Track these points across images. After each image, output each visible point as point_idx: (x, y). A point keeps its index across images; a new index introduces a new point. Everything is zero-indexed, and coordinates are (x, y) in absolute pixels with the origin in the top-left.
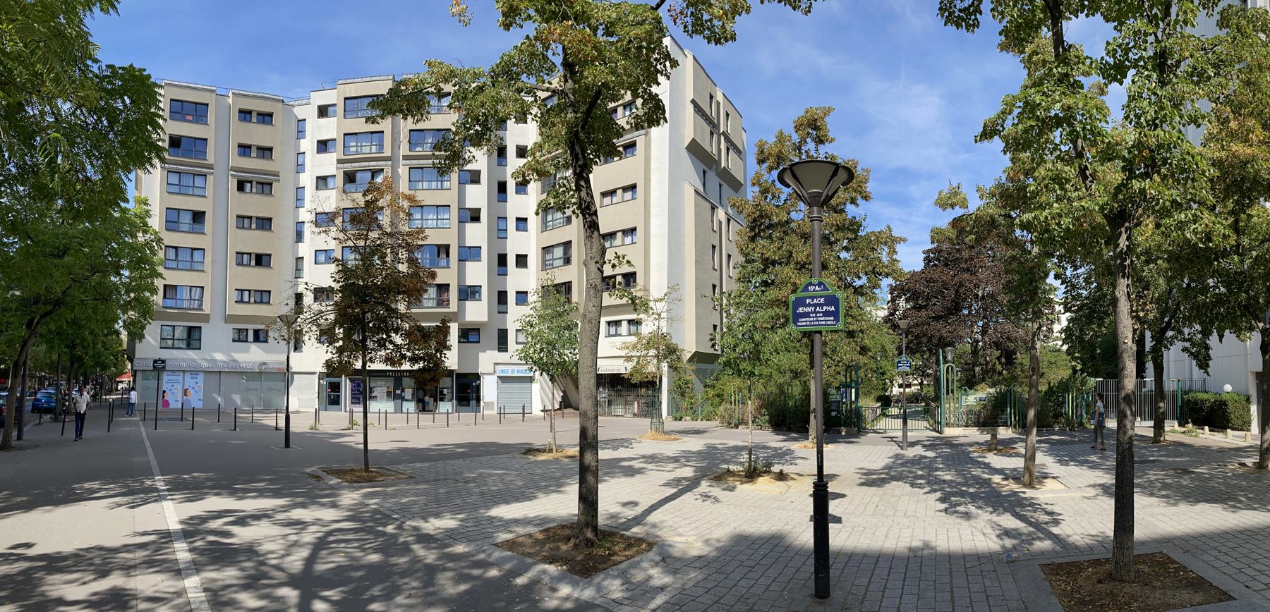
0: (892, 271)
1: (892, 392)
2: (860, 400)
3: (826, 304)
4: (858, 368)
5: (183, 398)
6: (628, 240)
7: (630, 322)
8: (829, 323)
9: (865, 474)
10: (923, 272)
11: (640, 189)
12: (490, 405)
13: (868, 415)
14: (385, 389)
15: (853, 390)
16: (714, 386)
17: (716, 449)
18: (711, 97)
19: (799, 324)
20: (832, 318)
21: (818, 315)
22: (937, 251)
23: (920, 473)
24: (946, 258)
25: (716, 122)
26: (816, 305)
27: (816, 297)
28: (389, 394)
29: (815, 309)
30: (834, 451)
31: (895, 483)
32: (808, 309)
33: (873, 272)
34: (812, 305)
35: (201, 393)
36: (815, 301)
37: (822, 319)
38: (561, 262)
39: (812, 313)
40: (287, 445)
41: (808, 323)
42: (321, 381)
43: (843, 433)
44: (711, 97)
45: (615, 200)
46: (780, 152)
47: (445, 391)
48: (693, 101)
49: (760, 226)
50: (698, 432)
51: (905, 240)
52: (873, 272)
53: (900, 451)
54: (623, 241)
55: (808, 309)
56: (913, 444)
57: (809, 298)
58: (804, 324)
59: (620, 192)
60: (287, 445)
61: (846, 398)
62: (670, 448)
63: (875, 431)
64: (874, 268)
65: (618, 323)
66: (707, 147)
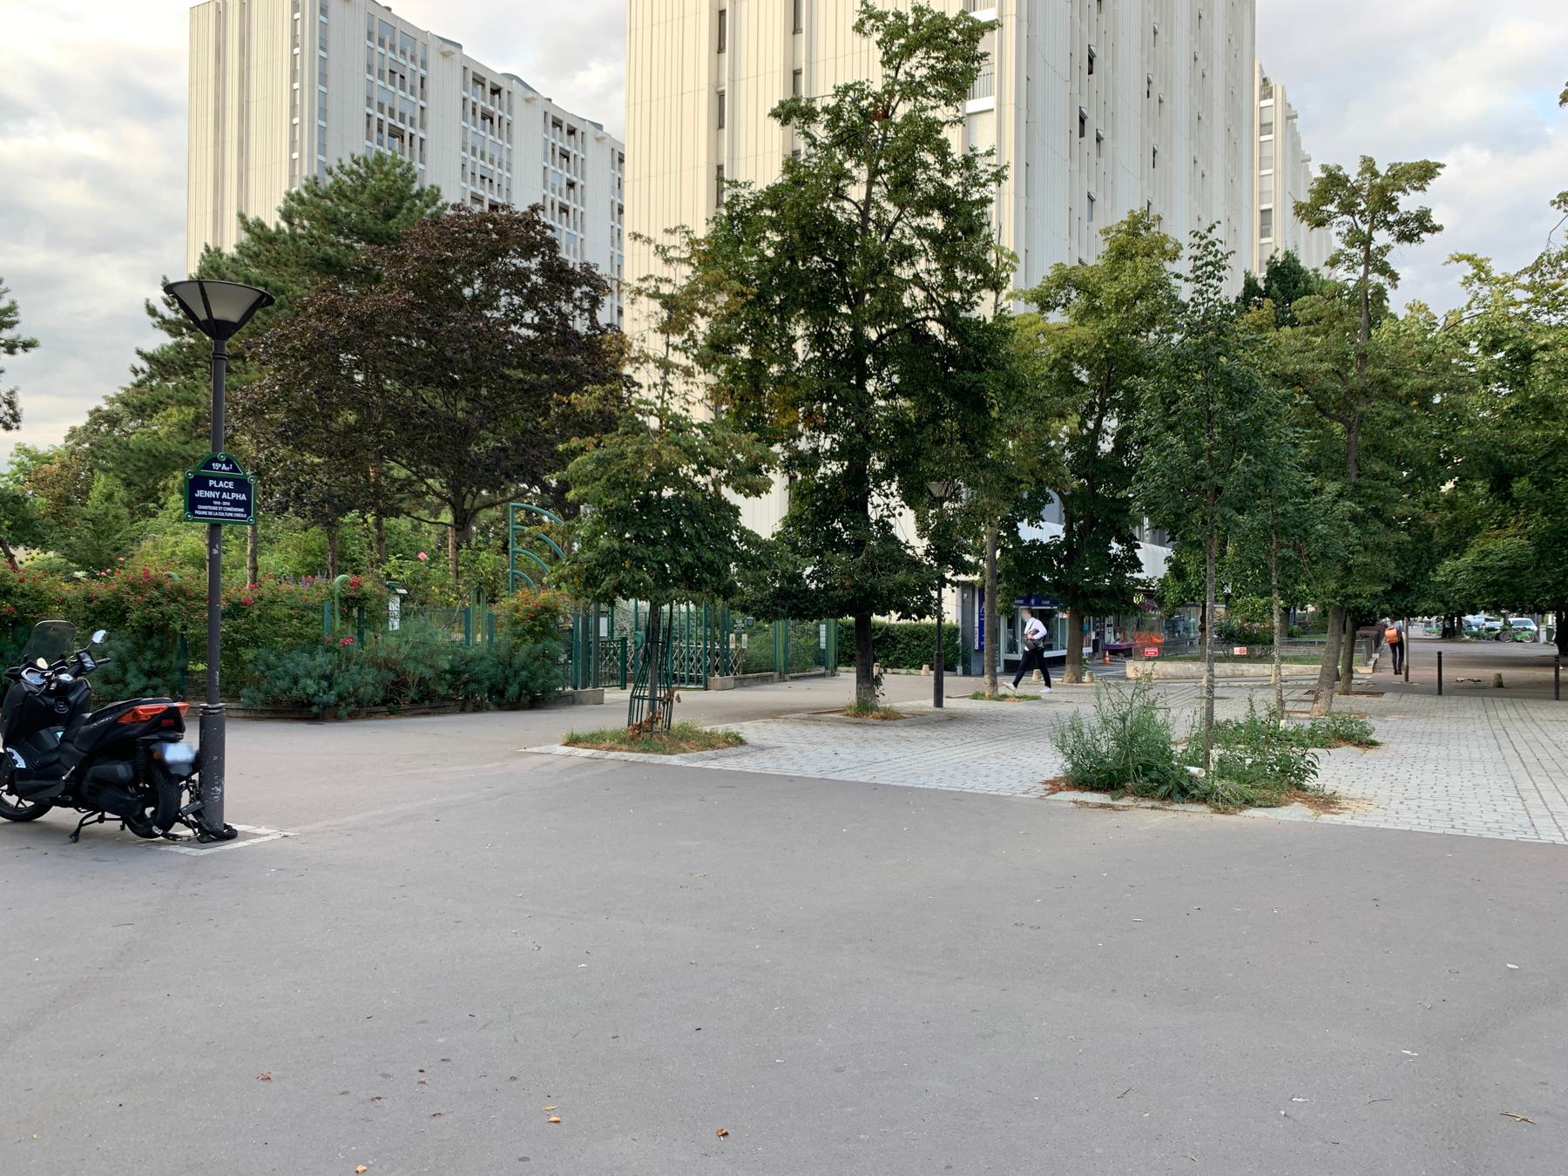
26: (222, 490)
32: (210, 494)
39: (216, 499)
55: (210, 494)
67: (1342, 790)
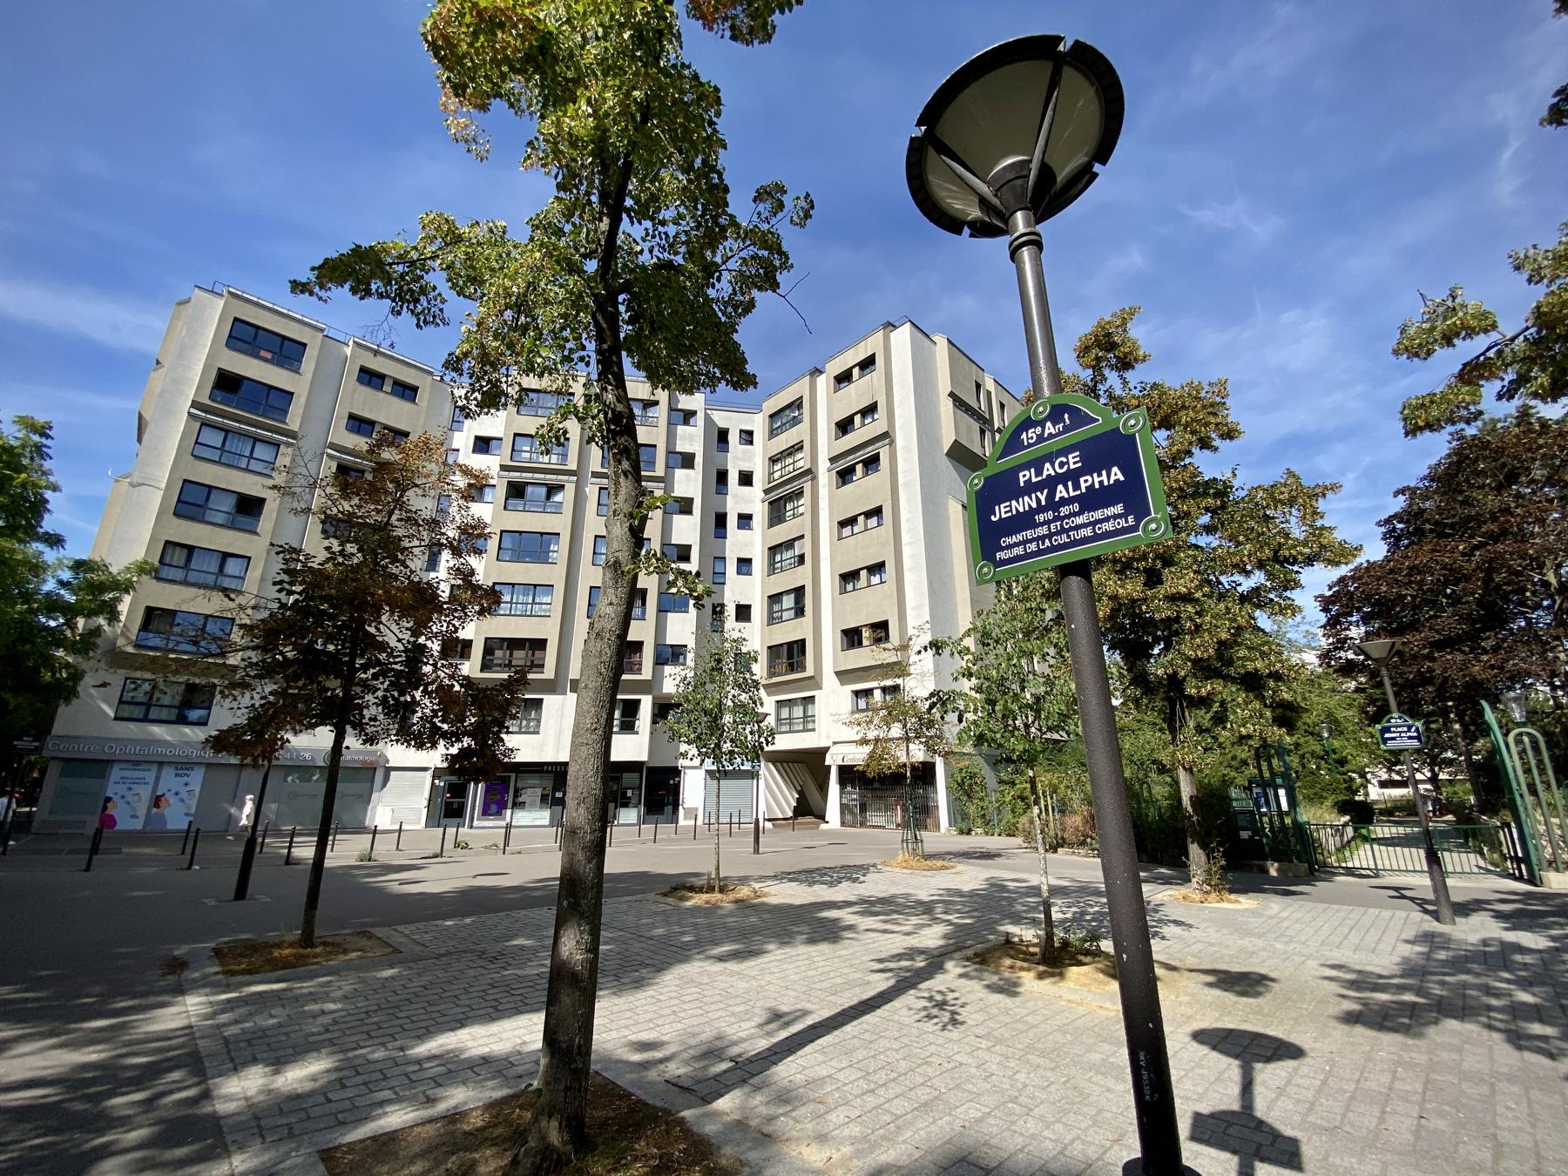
0: (1323, 551)
1: (1367, 794)
2: (1300, 810)
3: (1089, 467)
4: (1281, 751)
5: (149, 809)
6: (875, 579)
7: (884, 690)
8: (1109, 526)
9: (1353, 985)
10: (1387, 559)
11: (887, 513)
12: (692, 814)
13: (1330, 842)
14: (539, 791)
15: (1282, 792)
16: (1013, 784)
17: (1004, 888)
18: (978, 386)
19: (1000, 555)
21: (1064, 511)
22: (1411, 516)
23: (1525, 997)
24: (1437, 523)
26: (1051, 483)
27: (1050, 459)
28: (544, 798)
29: (1051, 496)
30: (1253, 913)
31: (1452, 1024)
32: (1027, 502)
33: (1276, 559)
34: (1039, 487)
35: (193, 803)
36: (1048, 470)
37: (1079, 520)
38: (792, 613)
39: (1041, 509)
40: (241, 892)
41: (1033, 547)
42: (436, 781)
43: (1273, 873)
44: (978, 386)
45: (856, 530)
47: (629, 793)
48: (952, 395)
50: (987, 856)
51: (1334, 488)
52: (1276, 559)
53: (1434, 926)
54: (869, 580)
55: (1027, 502)
56: (1465, 909)
57: (1026, 466)
58: (1019, 551)
59: (861, 519)
60: (241, 892)
61: (1268, 804)
62: (926, 885)
63: (1350, 872)
64: (1276, 552)
65: (868, 693)
66: (977, 450)
67: (1305, 1047)
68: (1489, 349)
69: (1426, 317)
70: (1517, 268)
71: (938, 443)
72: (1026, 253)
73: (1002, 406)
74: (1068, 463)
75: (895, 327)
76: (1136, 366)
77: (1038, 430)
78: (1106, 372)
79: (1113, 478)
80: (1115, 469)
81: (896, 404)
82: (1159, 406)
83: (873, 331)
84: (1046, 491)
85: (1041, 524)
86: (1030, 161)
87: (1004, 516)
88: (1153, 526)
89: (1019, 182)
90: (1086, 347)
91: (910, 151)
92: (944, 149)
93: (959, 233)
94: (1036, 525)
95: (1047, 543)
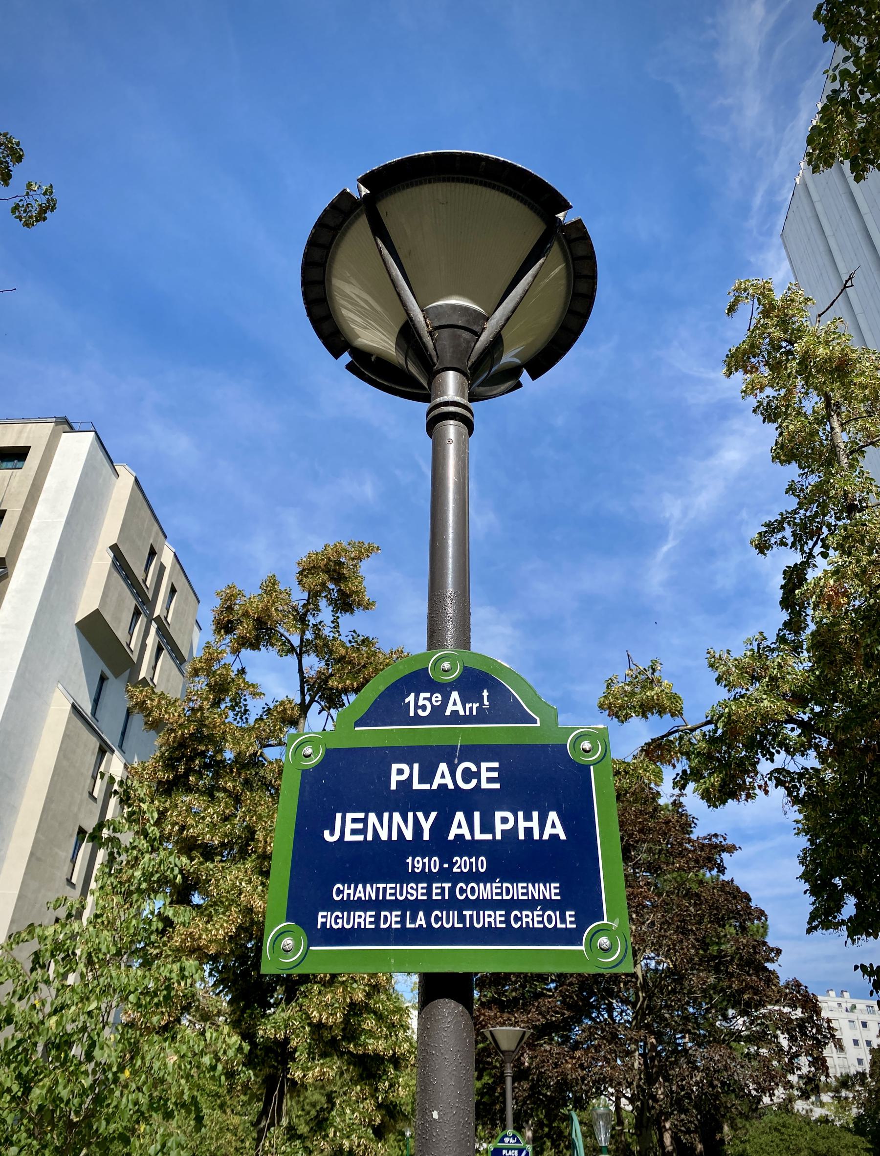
8: (531, 919)
18: (152, 553)
19: (325, 918)
20: (551, 891)
21: (461, 864)
25: (150, 596)
29: (442, 826)
36: (443, 776)
37: (485, 891)
39: (418, 847)
41: (392, 919)
44: (152, 553)
46: (267, 609)
48: (114, 548)
49: (191, 759)
57: (407, 755)
58: (364, 919)
66: (121, 634)
68: (670, 734)
69: (628, 680)
70: (711, 666)
71: (72, 604)
72: (452, 429)
73: (173, 591)
74: (477, 775)
75: (72, 430)
76: (356, 611)
77: (437, 698)
78: (323, 603)
79: (548, 831)
80: (553, 816)
81: (33, 526)
82: (364, 666)
83: (40, 419)
84: (433, 815)
85: (417, 878)
86: (487, 319)
87: (348, 837)
88: (604, 941)
89: (466, 335)
90: (314, 567)
91: (333, 206)
92: (379, 230)
93: (337, 355)
94: (404, 876)
95: (421, 921)
